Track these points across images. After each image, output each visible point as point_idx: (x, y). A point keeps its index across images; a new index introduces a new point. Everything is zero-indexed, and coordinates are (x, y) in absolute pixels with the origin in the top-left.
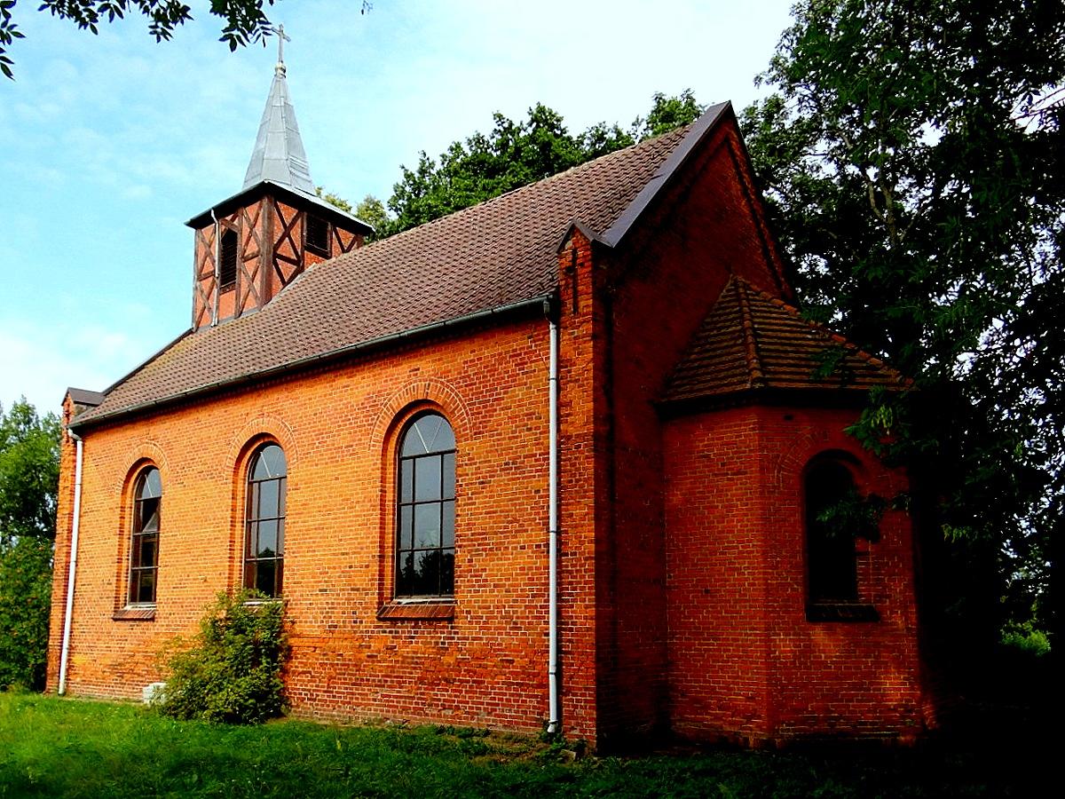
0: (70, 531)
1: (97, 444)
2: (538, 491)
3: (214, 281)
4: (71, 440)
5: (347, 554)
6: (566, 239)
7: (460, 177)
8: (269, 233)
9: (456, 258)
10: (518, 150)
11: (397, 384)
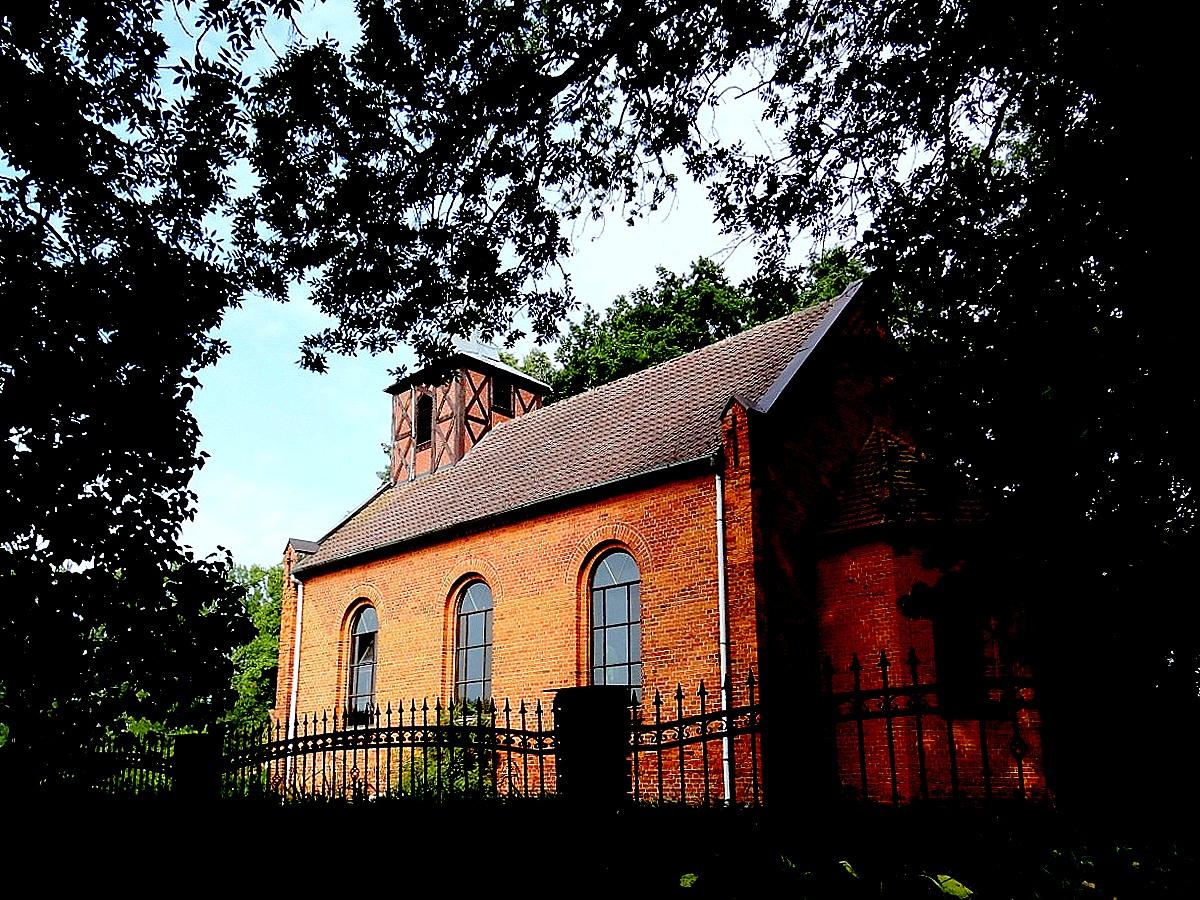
0: (291, 665)
1: (315, 587)
2: (710, 611)
3: (410, 441)
4: (292, 585)
5: (548, 671)
6: (728, 407)
7: (625, 330)
8: (462, 398)
9: (633, 418)
10: (681, 301)
11: (592, 526)
